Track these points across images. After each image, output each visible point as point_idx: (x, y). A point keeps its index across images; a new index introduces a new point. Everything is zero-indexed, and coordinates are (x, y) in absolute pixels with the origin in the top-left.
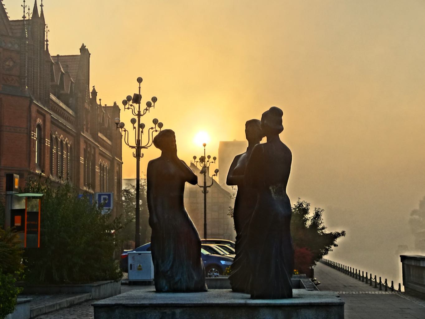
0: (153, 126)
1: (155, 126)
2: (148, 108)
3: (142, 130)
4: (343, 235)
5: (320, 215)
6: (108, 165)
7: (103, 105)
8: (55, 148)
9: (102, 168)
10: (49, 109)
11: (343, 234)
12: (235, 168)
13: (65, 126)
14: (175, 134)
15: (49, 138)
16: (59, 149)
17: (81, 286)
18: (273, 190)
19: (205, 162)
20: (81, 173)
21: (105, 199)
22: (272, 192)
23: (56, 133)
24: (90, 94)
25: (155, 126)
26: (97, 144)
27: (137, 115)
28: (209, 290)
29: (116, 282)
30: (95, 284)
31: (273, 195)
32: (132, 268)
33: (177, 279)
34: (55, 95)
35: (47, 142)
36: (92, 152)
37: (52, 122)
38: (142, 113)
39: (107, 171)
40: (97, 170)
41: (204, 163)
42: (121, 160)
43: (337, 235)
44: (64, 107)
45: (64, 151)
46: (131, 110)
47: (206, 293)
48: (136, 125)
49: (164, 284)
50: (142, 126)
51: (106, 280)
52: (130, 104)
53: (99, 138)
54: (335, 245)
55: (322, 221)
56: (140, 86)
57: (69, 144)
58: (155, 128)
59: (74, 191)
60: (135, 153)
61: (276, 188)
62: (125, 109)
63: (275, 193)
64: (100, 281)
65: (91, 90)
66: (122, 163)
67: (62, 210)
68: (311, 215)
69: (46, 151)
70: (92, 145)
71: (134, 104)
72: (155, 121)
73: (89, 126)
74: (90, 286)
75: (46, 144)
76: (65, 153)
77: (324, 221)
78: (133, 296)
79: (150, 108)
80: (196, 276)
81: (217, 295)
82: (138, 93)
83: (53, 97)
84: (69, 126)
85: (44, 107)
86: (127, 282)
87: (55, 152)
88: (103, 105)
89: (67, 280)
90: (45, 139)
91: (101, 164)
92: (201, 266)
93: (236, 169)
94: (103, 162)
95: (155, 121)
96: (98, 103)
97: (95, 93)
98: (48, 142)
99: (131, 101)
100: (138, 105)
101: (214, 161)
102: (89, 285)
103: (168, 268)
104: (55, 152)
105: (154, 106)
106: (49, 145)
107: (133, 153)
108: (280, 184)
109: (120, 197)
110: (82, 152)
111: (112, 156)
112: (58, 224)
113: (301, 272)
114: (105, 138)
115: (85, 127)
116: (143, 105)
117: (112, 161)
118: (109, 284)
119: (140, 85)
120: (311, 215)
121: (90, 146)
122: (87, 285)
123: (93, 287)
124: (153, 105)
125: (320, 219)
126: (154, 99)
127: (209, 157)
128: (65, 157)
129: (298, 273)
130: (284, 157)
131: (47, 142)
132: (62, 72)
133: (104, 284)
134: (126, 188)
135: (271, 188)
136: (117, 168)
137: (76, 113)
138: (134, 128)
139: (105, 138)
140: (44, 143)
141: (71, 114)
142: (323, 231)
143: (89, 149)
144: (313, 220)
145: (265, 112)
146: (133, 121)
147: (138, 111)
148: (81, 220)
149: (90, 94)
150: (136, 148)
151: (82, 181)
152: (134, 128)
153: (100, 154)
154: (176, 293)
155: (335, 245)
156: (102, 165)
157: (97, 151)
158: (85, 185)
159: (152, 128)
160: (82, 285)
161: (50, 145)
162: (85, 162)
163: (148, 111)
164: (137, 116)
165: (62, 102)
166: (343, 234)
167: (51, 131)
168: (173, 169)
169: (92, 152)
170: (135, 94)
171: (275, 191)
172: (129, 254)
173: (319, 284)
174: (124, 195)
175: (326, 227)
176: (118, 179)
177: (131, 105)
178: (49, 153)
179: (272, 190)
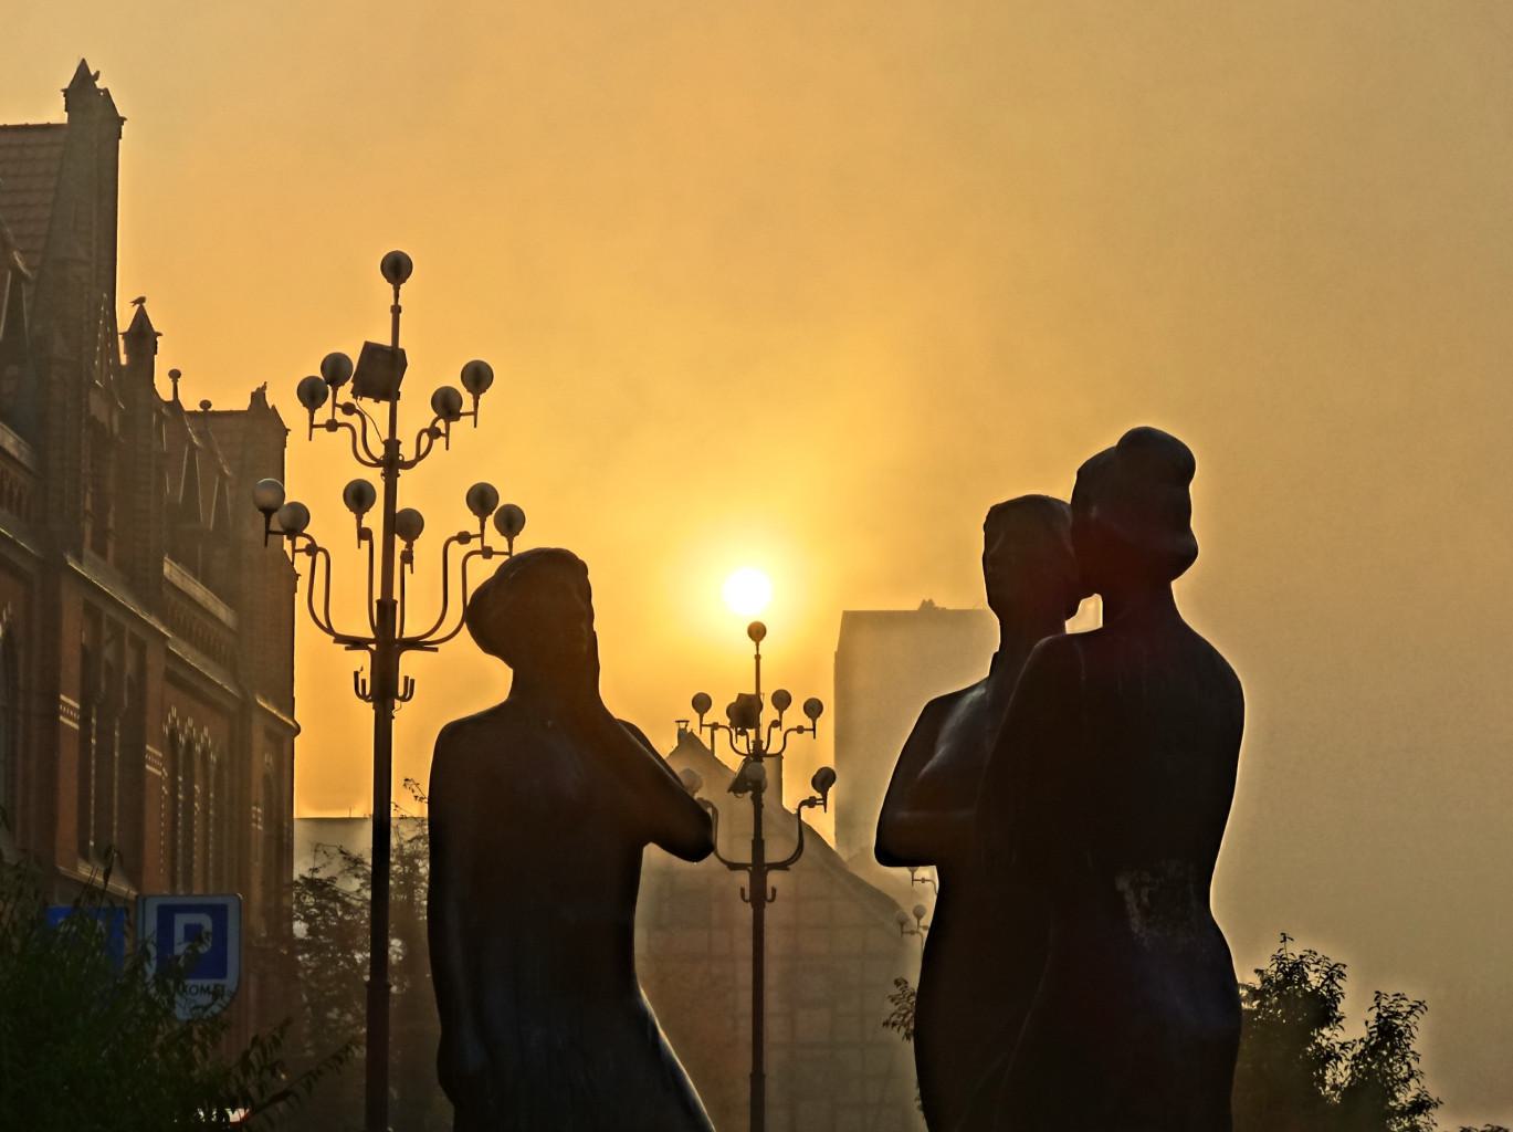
0: (471, 523)
1: (482, 527)
2: (441, 424)
3: (410, 546)
5: (1401, 1034)
7: (190, 403)
9: (179, 755)
12: (925, 770)
19: (756, 726)
21: (193, 933)
22: (1132, 907)
25: (482, 527)
26: (153, 621)
27: (378, 463)
31: (1136, 923)
36: (130, 667)
38: (407, 452)
41: (751, 732)
48: (374, 519)
50: (405, 525)
52: (340, 401)
58: (482, 536)
60: (366, 675)
65: (125, 318)
66: (298, 731)
68: (1352, 1027)
70: (129, 626)
71: (366, 404)
72: (481, 499)
73: (111, 524)
79: (452, 424)
82: (387, 341)
88: (190, 403)
94: (190, 722)
95: (481, 499)
96: (164, 388)
97: (143, 336)
99: (349, 385)
100: (385, 405)
101: (808, 723)
105: (475, 413)
107: (356, 674)
110: (71, 669)
111: (240, 687)
115: (88, 528)
116: (415, 411)
119: (397, 296)
124: (467, 405)
125: (1404, 1057)
126: (478, 377)
127: (782, 700)
134: (315, 870)
135: (1122, 884)
136: (268, 758)
138: (364, 534)
141: (13, 451)
142: (1421, 1119)
143: (108, 653)
146: (358, 497)
150: (373, 646)
151: (67, 826)
152: (364, 534)
153: (170, 677)
159: (464, 538)
162: (84, 721)
163: (440, 442)
164: (381, 469)
169: (130, 667)
170: (370, 350)
171: (1146, 900)
174: (303, 908)
177: (348, 409)
179: (1130, 897)
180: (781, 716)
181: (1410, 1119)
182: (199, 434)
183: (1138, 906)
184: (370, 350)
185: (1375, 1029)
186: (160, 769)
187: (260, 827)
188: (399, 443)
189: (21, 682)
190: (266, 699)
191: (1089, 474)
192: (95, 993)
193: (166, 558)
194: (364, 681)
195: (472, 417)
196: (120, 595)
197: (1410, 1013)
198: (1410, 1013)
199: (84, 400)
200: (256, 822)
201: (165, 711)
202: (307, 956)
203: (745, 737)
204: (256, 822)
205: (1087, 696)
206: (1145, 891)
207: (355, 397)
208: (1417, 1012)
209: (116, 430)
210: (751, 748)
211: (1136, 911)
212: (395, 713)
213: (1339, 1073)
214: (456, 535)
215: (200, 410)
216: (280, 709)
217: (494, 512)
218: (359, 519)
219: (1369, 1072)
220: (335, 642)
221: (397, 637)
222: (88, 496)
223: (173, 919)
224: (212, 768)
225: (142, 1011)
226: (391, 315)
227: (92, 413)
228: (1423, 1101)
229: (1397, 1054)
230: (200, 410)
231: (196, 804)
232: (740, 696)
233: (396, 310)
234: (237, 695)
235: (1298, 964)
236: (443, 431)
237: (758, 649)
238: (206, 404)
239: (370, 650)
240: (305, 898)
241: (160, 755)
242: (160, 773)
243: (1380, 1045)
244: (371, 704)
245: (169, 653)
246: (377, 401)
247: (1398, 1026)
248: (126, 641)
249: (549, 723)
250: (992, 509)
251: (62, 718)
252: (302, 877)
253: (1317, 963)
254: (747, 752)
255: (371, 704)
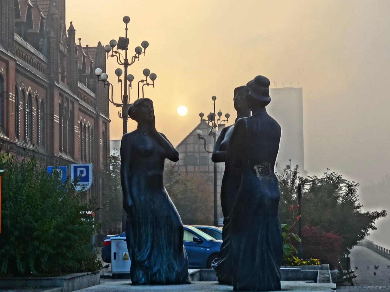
0: (144, 78)
1: (147, 79)
2: (137, 55)
3: (131, 83)
4: (383, 215)
5: (354, 191)
6: (91, 124)
7: (83, 45)
8: (22, 103)
9: (83, 128)
10: (14, 54)
11: (384, 214)
12: (222, 143)
13: (34, 75)
14: (153, 104)
15: (14, 92)
16: (27, 105)
17: (51, 279)
18: (259, 170)
19: (214, 120)
20: (55, 135)
21: (82, 172)
22: (257, 172)
23: (23, 84)
24: (67, 32)
25: (147, 79)
26: (76, 97)
27: (123, 64)
28: (192, 282)
29: (94, 275)
30: (68, 277)
31: (258, 175)
32: (116, 257)
33: (155, 269)
34: (20, 35)
35: (11, 96)
36: (70, 108)
37: (17, 71)
38: (130, 62)
39: (90, 133)
40: (77, 131)
41: (213, 121)
42: (109, 118)
43: (377, 215)
44: (33, 50)
45: (33, 108)
46: (115, 57)
47: (189, 285)
48: (122, 77)
49: (141, 276)
51: (82, 271)
52: (114, 50)
53: (79, 90)
54: (374, 228)
55: (357, 197)
56: (127, 28)
57: (40, 98)
58: (146, 80)
59: (41, 166)
60: (121, 112)
61: (262, 167)
62: (108, 57)
63: (260, 173)
64: (74, 273)
65: (68, 27)
66: (110, 121)
67: (27, 189)
68: (344, 189)
69: (10, 108)
70: (70, 98)
71: (120, 51)
72: (146, 72)
73: (65, 75)
74: (62, 279)
75: (10, 99)
76: (35, 109)
77: (359, 198)
78: (104, 288)
79: (140, 55)
80: (177, 266)
81: (199, 288)
82: (124, 36)
83: (17, 37)
84: (40, 74)
85: (7, 51)
86: (111, 274)
87: (22, 109)
88: (83, 45)
89: (34, 272)
90: (8, 93)
91: (81, 123)
92: (184, 255)
93: (223, 143)
94: (85, 120)
95: (146, 72)
96: (77, 42)
97: (72, 31)
98: (12, 96)
99: (116, 47)
100: (124, 51)
101: (226, 119)
102: (60, 277)
103: (146, 257)
104: (22, 109)
105: (145, 53)
106: (14, 101)
107: (119, 112)
108: (266, 163)
109: (107, 166)
110: (57, 108)
111: (97, 112)
112: (23, 205)
113: (323, 262)
114: (86, 89)
115: (60, 76)
116: (131, 51)
117: (96, 119)
118: (85, 277)
119: (127, 26)
120: (344, 189)
121: (67, 100)
122: (58, 277)
123: (65, 280)
124: (143, 51)
125: (354, 196)
126: (145, 44)
127: (220, 114)
128: (35, 115)
129: (319, 264)
130: (273, 131)
131: (11, 96)
132: (29, 5)
133: (79, 277)
134: (114, 154)
135: (255, 167)
136: (104, 128)
137: (48, 57)
138: (120, 81)
139: (86, 89)
140: (8, 98)
141: (42, 59)
142: (358, 210)
143: (65, 105)
144: (346, 197)
145: (165, 135)
146: (118, 72)
147: (124, 60)
148: (50, 201)
149: (67, 32)
150: (123, 106)
151: (57, 145)
152: (120, 81)
153: (80, 110)
154: (153, 285)
155: (374, 228)
156: (83, 124)
157: (76, 107)
158: (61, 150)
159: (143, 81)
160: (52, 278)
161: (15, 101)
162: (60, 120)
163: (137, 59)
164: (124, 66)
165: (30, 43)
166: (384, 214)
167: (16, 82)
168: (150, 144)
169: (70, 108)
170: (121, 38)
171: (260, 171)
172: (112, 240)
173: (356, 277)
174: (112, 163)
175: (361, 205)
176: (104, 142)
177: (116, 52)
178: (14, 110)
180: (220, 118)
181: (356, 210)
182: (85, 52)
183: (259, 172)
184: (121, 38)
185: (348, 189)
186: (78, 131)
187: (102, 144)
188: (128, 59)
189: (45, 112)
190: (103, 114)
191: (247, 85)
192: (57, 187)
193: (78, 82)
194: (121, 114)
195: (144, 54)
196: (68, 91)
197: (356, 186)
198: (356, 186)
199: (58, 46)
200: (101, 143)
201: (79, 118)
202: (113, 174)
203: (212, 123)
204: (101, 143)
205: (252, 130)
206: (260, 169)
207: (118, 49)
208: (357, 186)
209: (66, 53)
210: (213, 125)
211: (258, 173)
212: (128, 121)
213: (340, 201)
214: (141, 80)
215: (86, 47)
216: (106, 116)
217: (149, 75)
218: (119, 77)
219: (346, 199)
220: (114, 105)
221: (128, 103)
222: (60, 69)
223: (77, 169)
224: (90, 131)
225: (68, 191)
226: (125, 31)
227: (60, 49)
228: (359, 206)
229: (324, 199)
230: (86, 47)
231: (87, 139)
232: (210, 113)
233: (127, 29)
234: (96, 113)
235: (331, 175)
236: (138, 57)
237: (214, 102)
238: (87, 46)
239: (122, 107)
240: (112, 160)
241: (78, 128)
242: (78, 132)
243: (349, 193)
244: (122, 119)
245: (80, 104)
246: (123, 50)
247: (353, 189)
248: (69, 102)
249: (145, 134)
250: (235, 89)
251: (58, 117)
252: (111, 156)
253: (335, 175)
254: (212, 126)
255: (122, 119)
